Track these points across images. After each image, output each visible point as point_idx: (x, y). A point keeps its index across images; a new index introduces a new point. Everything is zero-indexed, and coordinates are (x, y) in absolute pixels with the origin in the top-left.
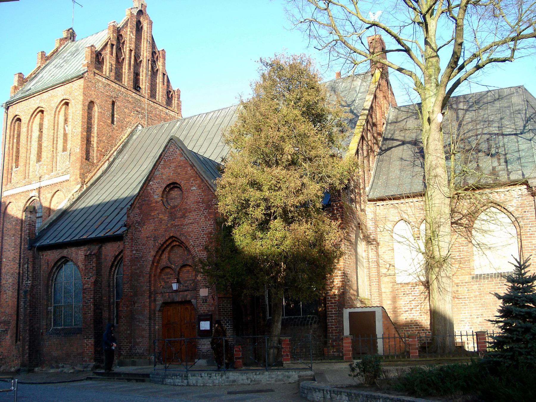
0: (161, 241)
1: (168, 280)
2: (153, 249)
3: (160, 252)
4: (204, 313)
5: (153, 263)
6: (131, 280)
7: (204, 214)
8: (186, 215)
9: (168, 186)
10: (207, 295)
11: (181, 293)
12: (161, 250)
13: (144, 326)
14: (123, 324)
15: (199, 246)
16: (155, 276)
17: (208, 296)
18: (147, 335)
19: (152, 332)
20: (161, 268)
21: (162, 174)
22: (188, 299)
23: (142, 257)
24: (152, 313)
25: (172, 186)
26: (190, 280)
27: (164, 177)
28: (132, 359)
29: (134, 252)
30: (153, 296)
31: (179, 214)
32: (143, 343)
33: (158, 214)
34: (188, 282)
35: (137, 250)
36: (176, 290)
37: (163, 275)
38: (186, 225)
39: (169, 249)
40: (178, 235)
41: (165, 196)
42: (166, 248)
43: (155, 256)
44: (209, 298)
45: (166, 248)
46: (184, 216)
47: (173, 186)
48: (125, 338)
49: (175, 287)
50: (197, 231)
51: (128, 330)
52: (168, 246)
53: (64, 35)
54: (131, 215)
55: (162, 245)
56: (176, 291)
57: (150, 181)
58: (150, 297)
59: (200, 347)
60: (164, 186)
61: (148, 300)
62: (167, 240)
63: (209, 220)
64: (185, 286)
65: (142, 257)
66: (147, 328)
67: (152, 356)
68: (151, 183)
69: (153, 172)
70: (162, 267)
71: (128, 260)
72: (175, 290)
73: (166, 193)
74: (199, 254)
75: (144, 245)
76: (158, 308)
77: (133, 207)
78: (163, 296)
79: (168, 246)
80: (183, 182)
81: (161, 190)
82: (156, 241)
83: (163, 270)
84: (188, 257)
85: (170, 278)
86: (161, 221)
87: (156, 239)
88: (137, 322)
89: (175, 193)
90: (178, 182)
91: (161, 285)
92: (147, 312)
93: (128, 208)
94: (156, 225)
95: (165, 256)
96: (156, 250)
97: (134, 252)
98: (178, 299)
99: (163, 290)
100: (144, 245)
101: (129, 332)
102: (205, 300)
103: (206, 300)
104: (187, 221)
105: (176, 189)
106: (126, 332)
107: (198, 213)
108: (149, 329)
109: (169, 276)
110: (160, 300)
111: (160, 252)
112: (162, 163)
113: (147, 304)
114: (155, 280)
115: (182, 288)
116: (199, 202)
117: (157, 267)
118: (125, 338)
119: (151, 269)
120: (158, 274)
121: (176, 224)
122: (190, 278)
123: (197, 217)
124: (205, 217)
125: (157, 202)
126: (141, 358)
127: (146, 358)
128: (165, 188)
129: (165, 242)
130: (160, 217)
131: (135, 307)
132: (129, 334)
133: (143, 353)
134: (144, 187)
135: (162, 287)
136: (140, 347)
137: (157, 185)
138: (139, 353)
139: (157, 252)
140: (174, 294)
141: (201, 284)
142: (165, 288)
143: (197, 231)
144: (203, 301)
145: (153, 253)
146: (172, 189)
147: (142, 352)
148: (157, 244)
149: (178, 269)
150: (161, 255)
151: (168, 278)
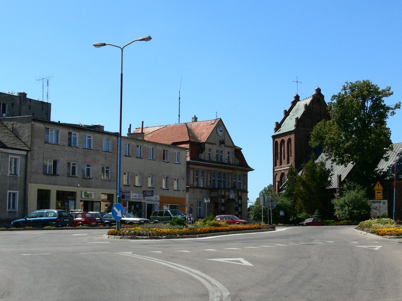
53: (293, 99)
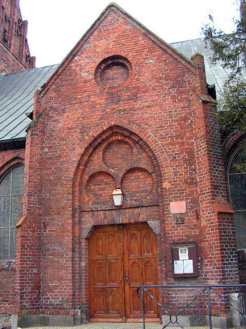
0: (94, 133)
1: (101, 192)
2: (78, 144)
3: (91, 150)
4: (180, 240)
5: (79, 165)
6: (40, 191)
7: (171, 93)
8: (139, 95)
9: (105, 61)
10: (184, 211)
11: (127, 210)
12: (94, 146)
13: (63, 261)
14: (27, 258)
15: (165, 138)
16: (80, 185)
17: (186, 213)
18: (70, 276)
19: (77, 272)
20: (90, 174)
21: (95, 46)
22: (141, 220)
23: (60, 156)
24: (76, 241)
25: (110, 62)
26: (143, 191)
27: (98, 50)
28: (41, 315)
29: (46, 150)
30: (77, 215)
31: (126, 95)
32: (61, 289)
33: (89, 96)
34: (137, 195)
35: (50, 148)
36: (121, 206)
37: (91, 185)
38: (138, 109)
39: (104, 146)
40: (124, 123)
41: (99, 74)
42: (100, 144)
43: (83, 155)
44: (188, 216)
45: (100, 144)
46: (134, 97)
47: (114, 61)
48: (29, 280)
49: (118, 201)
50: (159, 116)
51: (34, 268)
52: (104, 141)
54: (44, 100)
55: (96, 139)
56: (119, 208)
57: (75, 56)
58: (73, 216)
59: (174, 295)
60: (100, 60)
61: (70, 221)
62: (104, 132)
63: (179, 101)
64: (135, 200)
65: (60, 156)
66: (69, 264)
67: (77, 310)
68: (76, 58)
69: (81, 45)
70: (92, 172)
71: (36, 160)
72: (116, 206)
73: (100, 70)
74: (165, 150)
75: (62, 139)
76: (85, 234)
77: (47, 89)
78: (94, 215)
79: (104, 141)
80: (131, 55)
81: (95, 65)
82: (85, 134)
83: (92, 176)
84: (139, 157)
85: (104, 189)
86: (93, 106)
87: (84, 130)
88: (50, 255)
89: (115, 73)
90: (122, 54)
91: (90, 200)
92: (68, 240)
93: (38, 91)
94: (85, 112)
95: (97, 158)
96: (86, 145)
97: (46, 150)
98: (121, 219)
99: (94, 207)
100: (62, 139)
101: (35, 271)
102: (180, 219)
103: (183, 220)
104: (139, 104)
105: (115, 67)
106: (32, 271)
107: (160, 92)
108: (73, 267)
109: (102, 186)
110: (89, 222)
111: (91, 150)
112: (96, 33)
113: (70, 228)
114: (81, 192)
115: (129, 202)
116: (161, 78)
117: (83, 170)
118: (29, 280)
119: (76, 174)
120: (85, 182)
121: (121, 108)
122: (142, 189)
123: (159, 97)
124: (173, 97)
125: (86, 82)
126: (58, 313)
127: (67, 314)
128: (100, 64)
129: (100, 136)
130: (91, 100)
131: (45, 231)
132: (35, 274)
133: (62, 305)
134: (66, 64)
135: (91, 202)
136: (56, 295)
137: (87, 60)
138: (53, 305)
139: (87, 149)
140: (114, 212)
141: (172, 194)
142: (98, 204)
143: (159, 116)
144: (177, 221)
145: (80, 150)
146: (108, 67)
147: (58, 303)
148: (86, 137)
149: (121, 175)
150: (91, 156)
151: (101, 190)
